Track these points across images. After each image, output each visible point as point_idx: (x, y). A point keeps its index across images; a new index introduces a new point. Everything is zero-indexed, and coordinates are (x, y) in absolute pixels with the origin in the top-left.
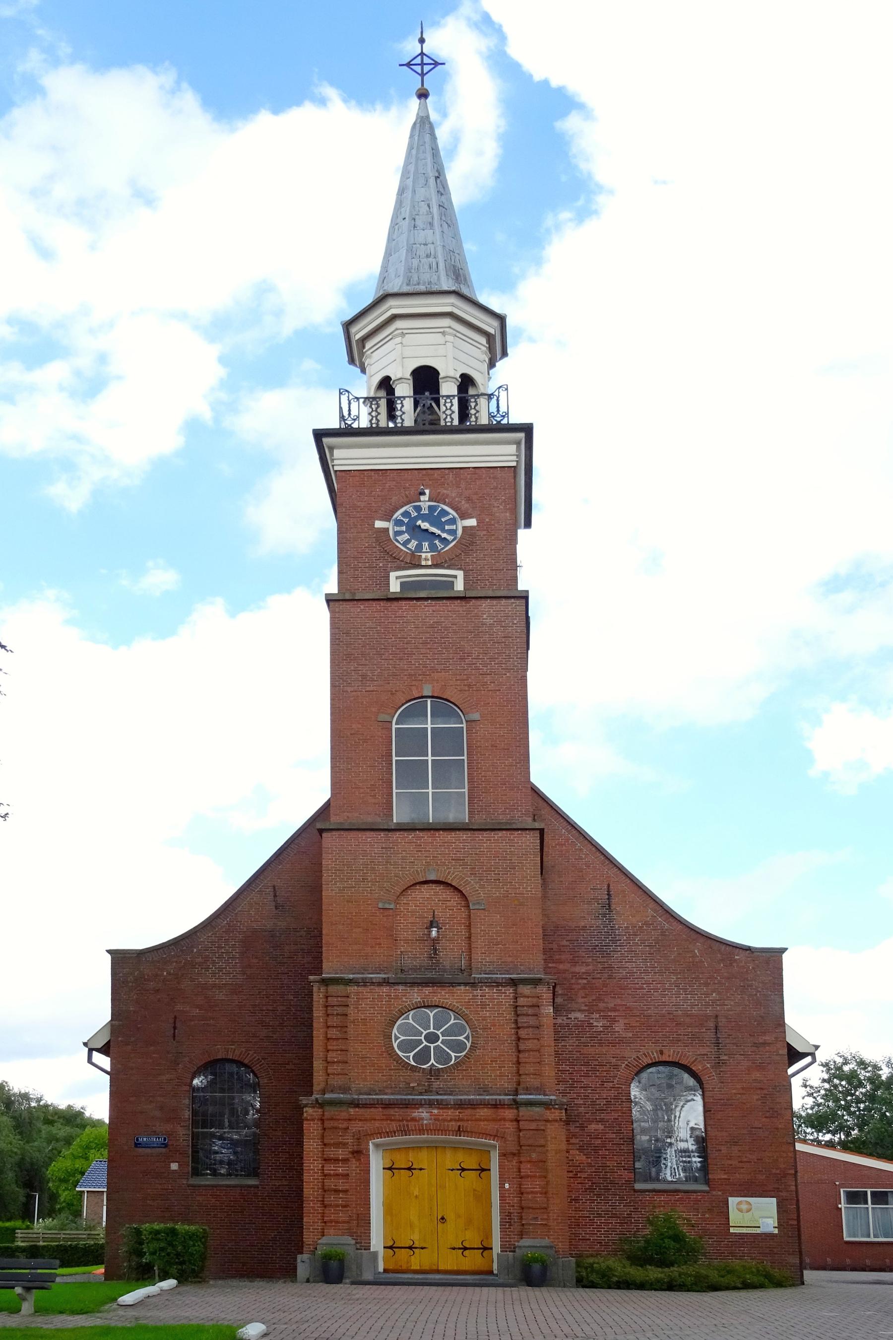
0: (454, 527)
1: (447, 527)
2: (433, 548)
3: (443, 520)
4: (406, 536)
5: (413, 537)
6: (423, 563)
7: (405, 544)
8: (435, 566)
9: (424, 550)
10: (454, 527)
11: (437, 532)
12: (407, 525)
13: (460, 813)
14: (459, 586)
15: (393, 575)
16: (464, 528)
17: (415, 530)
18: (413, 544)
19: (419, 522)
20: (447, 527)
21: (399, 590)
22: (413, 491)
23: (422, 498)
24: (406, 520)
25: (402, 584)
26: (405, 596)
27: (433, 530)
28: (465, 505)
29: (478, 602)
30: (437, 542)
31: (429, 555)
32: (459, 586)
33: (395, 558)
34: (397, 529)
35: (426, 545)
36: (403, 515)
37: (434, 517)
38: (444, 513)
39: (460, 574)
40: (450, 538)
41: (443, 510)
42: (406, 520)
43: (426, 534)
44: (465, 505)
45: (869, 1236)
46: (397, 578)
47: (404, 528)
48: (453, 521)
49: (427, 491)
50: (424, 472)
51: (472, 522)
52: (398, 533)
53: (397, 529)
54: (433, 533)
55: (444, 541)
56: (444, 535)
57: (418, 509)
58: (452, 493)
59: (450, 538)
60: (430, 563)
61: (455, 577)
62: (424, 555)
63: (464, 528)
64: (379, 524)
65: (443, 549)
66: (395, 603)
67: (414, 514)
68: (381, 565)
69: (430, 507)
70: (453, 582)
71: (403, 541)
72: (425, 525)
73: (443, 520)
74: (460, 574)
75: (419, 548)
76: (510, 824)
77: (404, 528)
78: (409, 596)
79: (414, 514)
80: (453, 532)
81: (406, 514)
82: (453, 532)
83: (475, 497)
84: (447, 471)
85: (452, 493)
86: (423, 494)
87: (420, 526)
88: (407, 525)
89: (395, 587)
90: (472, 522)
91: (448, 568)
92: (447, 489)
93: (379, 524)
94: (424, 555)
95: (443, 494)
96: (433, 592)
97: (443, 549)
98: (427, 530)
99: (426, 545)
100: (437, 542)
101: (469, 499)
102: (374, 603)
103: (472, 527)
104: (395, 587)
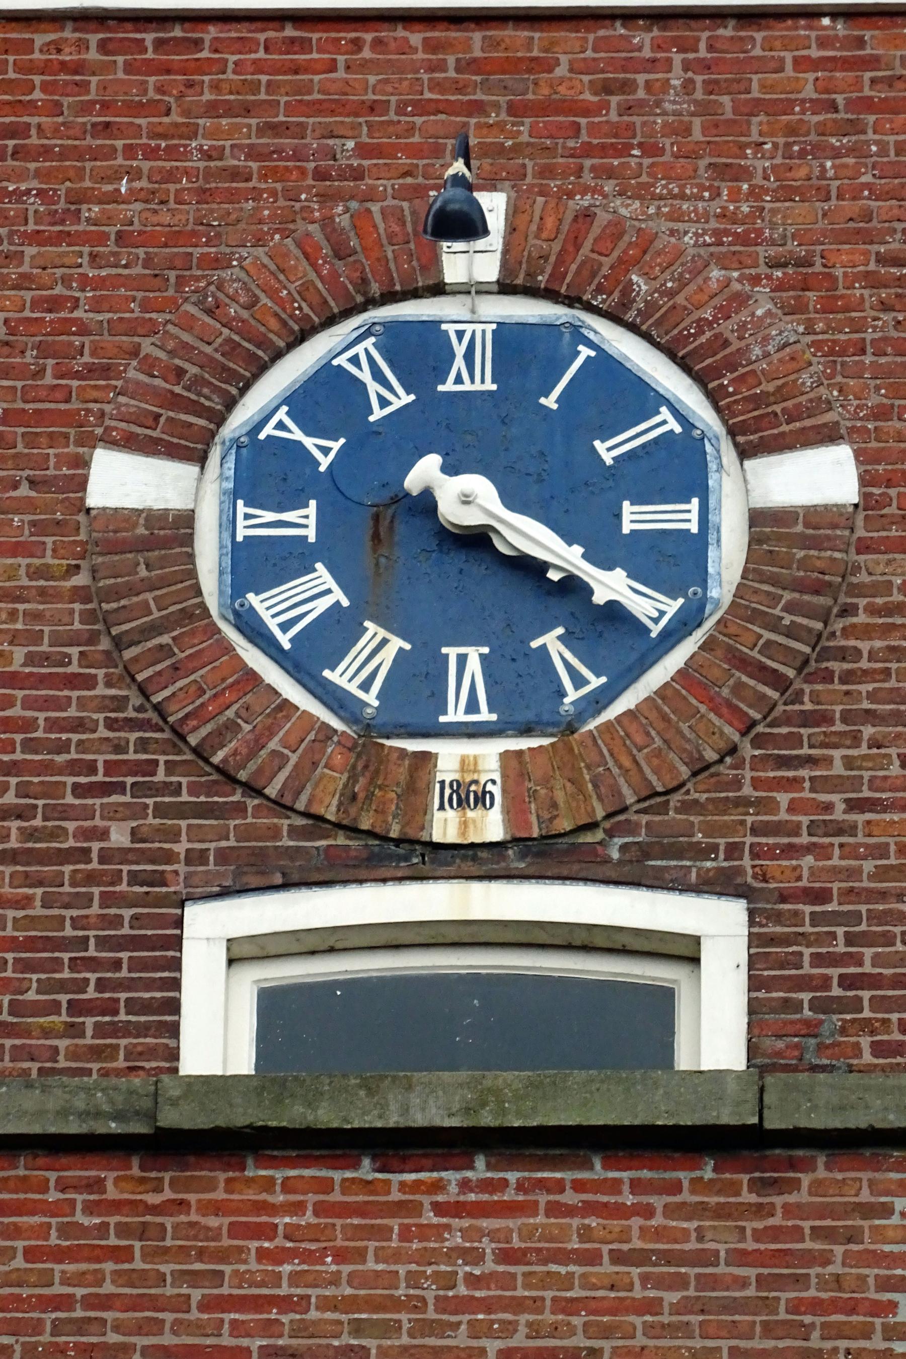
0: (685, 516)
1: (633, 517)
2: (521, 696)
3: (607, 451)
4: (320, 590)
5: (371, 600)
6: (445, 826)
7: (307, 659)
8: (537, 854)
9: (455, 714)
10: (685, 516)
11: (563, 555)
12: (332, 490)
13: (273, 796)
14: (714, 1031)
15: (209, 927)
16: (764, 522)
17: (389, 537)
18: (369, 662)
19: (426, 471)
20: (633, 517)
21: (244, 1062)
22: (388, 207)
23: (460, 262)
24: (324, 452)
25: (273, 1005)
26: (295, 1115)
27: (529, 535)
28: (770, 331)
29: (860, 1182)
30: (551, 641)
31: (489, 754)
32: (714, 1031)
33: (227, 776)
34: (256, 522)
35: (467, 666)
36: (304, 402)
37: (537, 433)
38: (617, 394)
39: (720, 925)
40: (650, 607)
41: (606, 365)
42: (324, 452)
43: (477, 569)
44: (770, 331)
45: (151, 613)
46: (240, 953)
47: (305, 521)
48: (677, 469)
49: (494, 205)
50: (476, 40)
51: (821, 477)
52: (260, 564)
53: (256, 522)
54: (529, 568)
55: (608, 633)
56: (610, 585)
57: (418, 354)
58: (676, 222)
59: (650, 607)
60: (491, 826)
61: (686, 952)
62: (449, 756)
63: (764, 522)
64: (122, 481)
65: (599, 701)
66: (218, 1182)
67: (389, 399)
68: (119, 837)
69: (508, 336)
70: (663, 1000)
71: (303, 639)
72: (467, 497)
73: (607, 451)
74: (720, 925)
75: (417, 690)
76: (269, 809)
77: (305, 521)
78: (326, 1116)
79: (389, 399)
80: (674, 561)
81: (327, 398)
82: (674, 561)
83: (846, 262)
84: (644, 39)
85: (676, 222)
86: (466, 225)
87: (426, 503)
88: (332, 490)
89: (217, 1033)
90: (821, 477)
91: (633, 875)
92: (643, 194)
93: (122, 481)
94: (449, 756)
95: (616, 230)
96: (510, 1079)
97: (599, 701)
98: (478, 540)
99: (467, 666)
100: (551, 641)
101: (801, 281)
102: (52, 1178)
103: (819, 520)
104: (217, 1033)
